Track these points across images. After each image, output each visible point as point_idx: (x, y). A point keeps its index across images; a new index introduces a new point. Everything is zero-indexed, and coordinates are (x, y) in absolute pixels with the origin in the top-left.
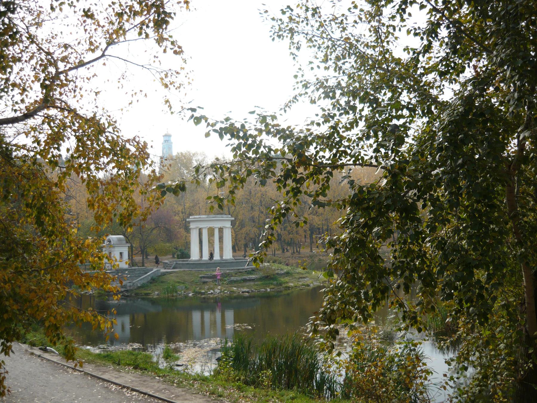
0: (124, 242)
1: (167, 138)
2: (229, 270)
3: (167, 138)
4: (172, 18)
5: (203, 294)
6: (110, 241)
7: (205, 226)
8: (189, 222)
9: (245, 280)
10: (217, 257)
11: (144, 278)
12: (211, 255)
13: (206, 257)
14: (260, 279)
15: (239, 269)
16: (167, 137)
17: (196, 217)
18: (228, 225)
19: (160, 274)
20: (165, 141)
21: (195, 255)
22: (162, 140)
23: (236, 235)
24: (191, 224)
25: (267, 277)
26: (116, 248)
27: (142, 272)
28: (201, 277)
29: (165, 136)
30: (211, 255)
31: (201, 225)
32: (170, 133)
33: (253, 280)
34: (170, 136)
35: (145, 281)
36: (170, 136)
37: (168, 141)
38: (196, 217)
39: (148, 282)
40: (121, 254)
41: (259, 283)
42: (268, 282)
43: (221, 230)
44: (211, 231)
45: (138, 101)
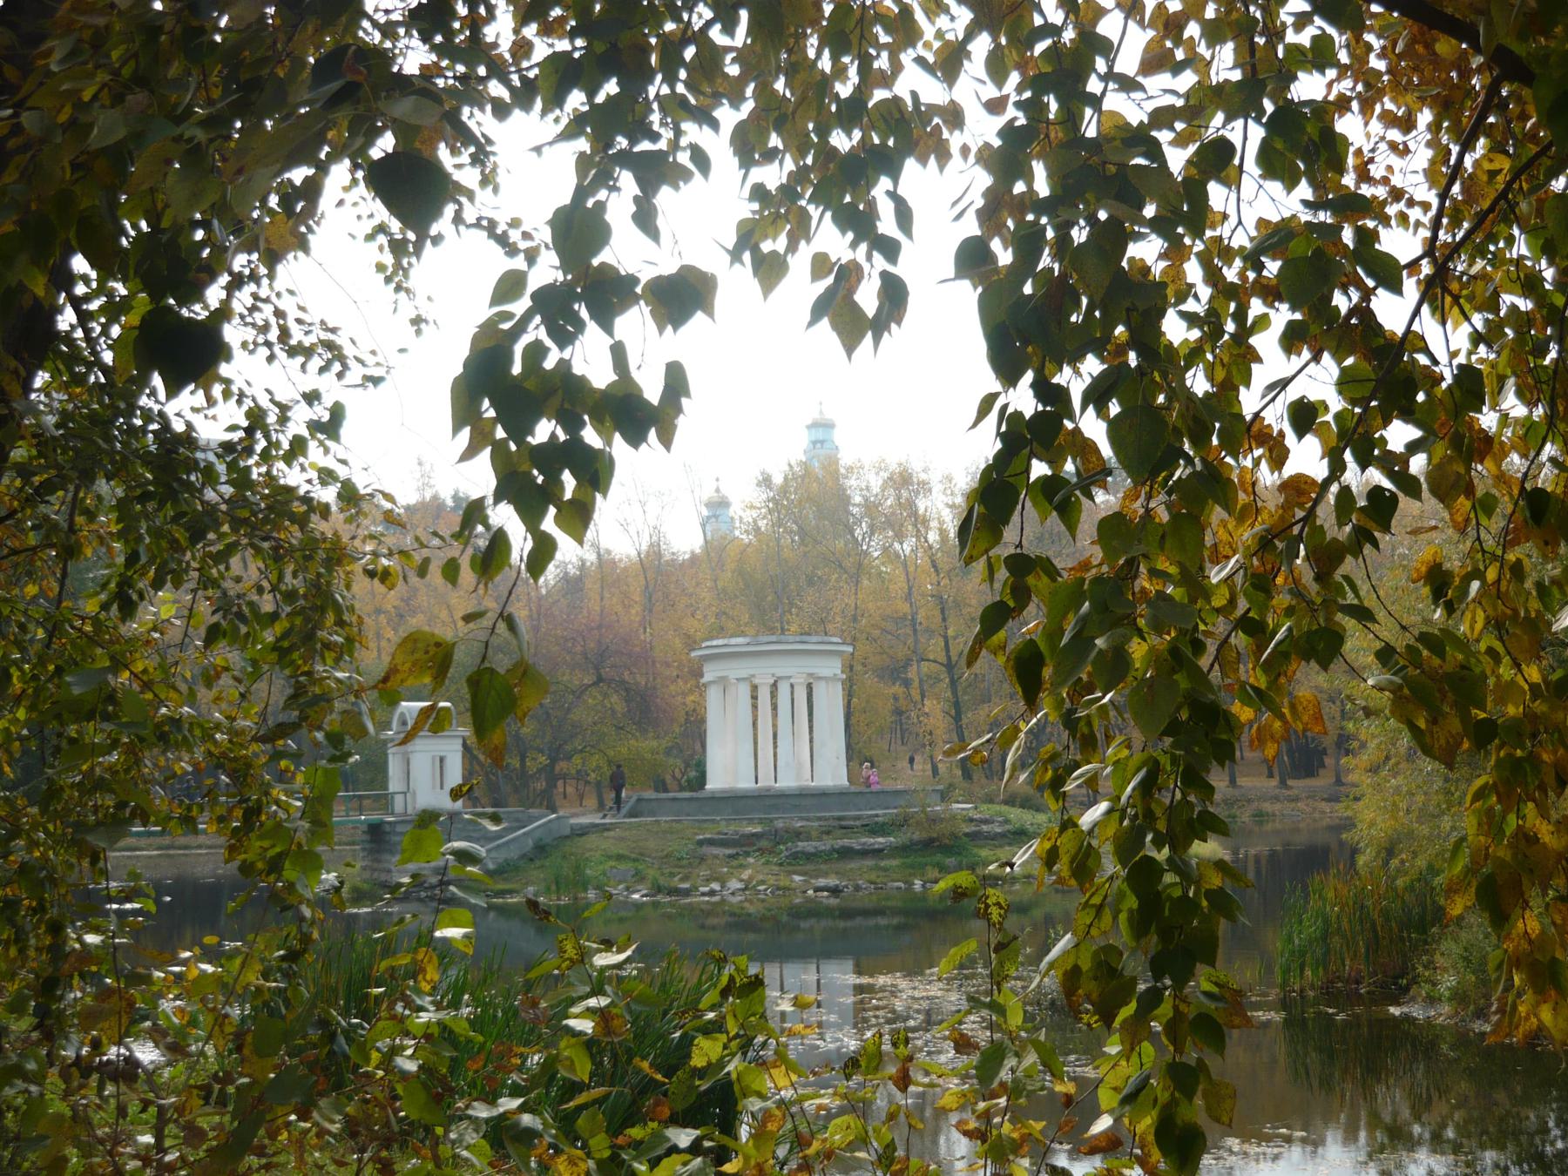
1: (819, 434)
2: (802, 819)
3: (819, 434)
4: (544, 112)
5: (687, 893)
9: (846, 853)
11: (507, 843)
14: (903, 850)
15: (840, 819)
17: (715, 643)
19: (567, 832)
20: (814, 443)
23: (849, 702)
25: (928, 845)
28: (701, 843)
29: (815, 425)
32: (829, 415)
33: (877, 853)
34: (829, 426)
35: (514, 853)
36: (829, 426)
37: (822, 442)
39: (523, 856)
41: (895, 862)
42: (924, 860)
45: (429, 298)
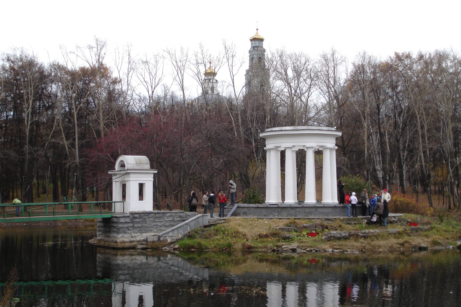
0: (148, 166)
1: (257, 43)
6: (123, 165)
7: (291, 145)
8: (264, 139)
10: (310, 198)
12: (302, 291)
13: (291, 199)
16: (257, 41)
18: (331, 144)
20: (254, 47)
21: (272, 197)
22: (248, 46)
24: (267, 142)
26: (131, 175)
27: (176, 219)
29: (253, 40)
30: (302, 291)
31: (284, 144)
38: (284, 128)
40: (141, 186)
43: (319, 153)
44: (301, 156)
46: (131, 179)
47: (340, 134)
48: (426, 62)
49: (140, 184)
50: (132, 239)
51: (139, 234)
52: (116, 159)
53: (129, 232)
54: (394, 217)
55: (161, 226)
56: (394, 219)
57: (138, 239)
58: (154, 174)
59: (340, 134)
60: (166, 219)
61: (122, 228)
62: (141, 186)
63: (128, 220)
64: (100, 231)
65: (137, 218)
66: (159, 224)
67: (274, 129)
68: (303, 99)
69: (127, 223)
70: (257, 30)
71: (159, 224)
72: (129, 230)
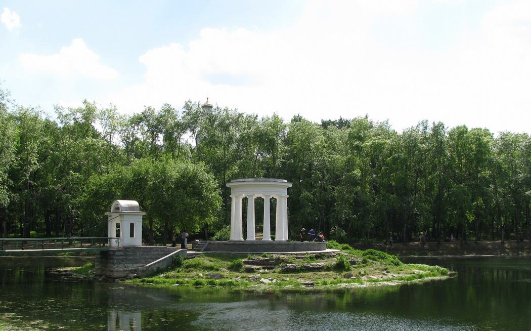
26: (125, 216)
40: (132, 225)
44: (259, 203)
46: (125, 219)
47: (290, 185)
48: (434, 324)
49: (131, 224)
50: (126, 269)
51: (131, 265)
52: (111, 203)
53: (123, 263)
54: (334, 252)
55: (148, 259)
56: (333, 254)
57: (130, 268)
58: (143, 216)
59: (290, 185)
60: (152, 253)
61: (117, 260)
62: (132, 225)
63: (121, 253)
64: (98, 261)
65: (129, 252)
66: (147, 257)
67: (238, 180)
68: (319, 127)
69: (121, 255)
70: (207, 99)
71: (147, 257)
72: (122, 261)
